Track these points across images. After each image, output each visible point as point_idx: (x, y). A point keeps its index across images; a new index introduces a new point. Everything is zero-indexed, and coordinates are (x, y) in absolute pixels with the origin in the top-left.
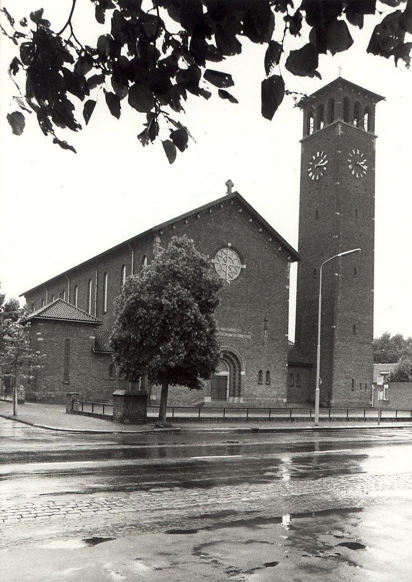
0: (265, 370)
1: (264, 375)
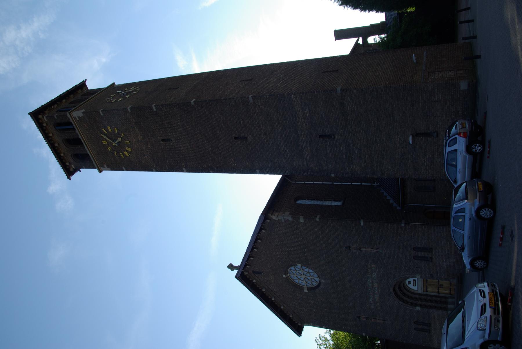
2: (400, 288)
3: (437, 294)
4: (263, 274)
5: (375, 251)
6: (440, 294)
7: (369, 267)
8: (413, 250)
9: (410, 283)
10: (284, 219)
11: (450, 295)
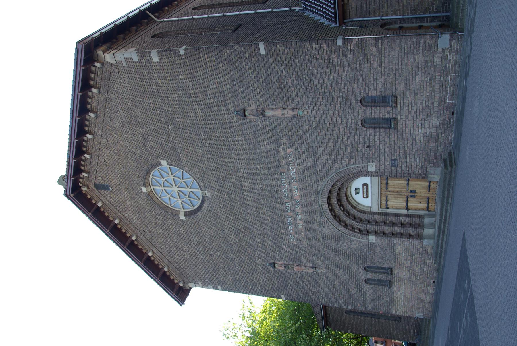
0: (361, 112)
2: (339, 200)
3: (405, 212)
4: (111, 188)
5: (291, 113)
6: (410, 211)
7: (282, 153)
8: (360, 104)
9: (357, 192)
10: (126, 59)
11: (427, 212)
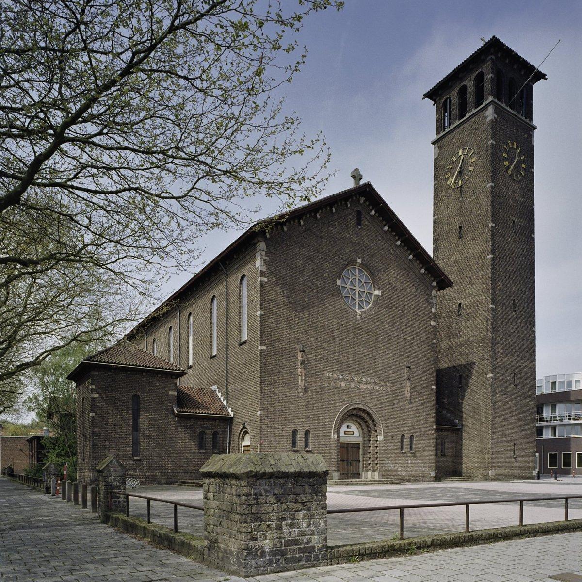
0: (408, 435)
1: (406, 441)
